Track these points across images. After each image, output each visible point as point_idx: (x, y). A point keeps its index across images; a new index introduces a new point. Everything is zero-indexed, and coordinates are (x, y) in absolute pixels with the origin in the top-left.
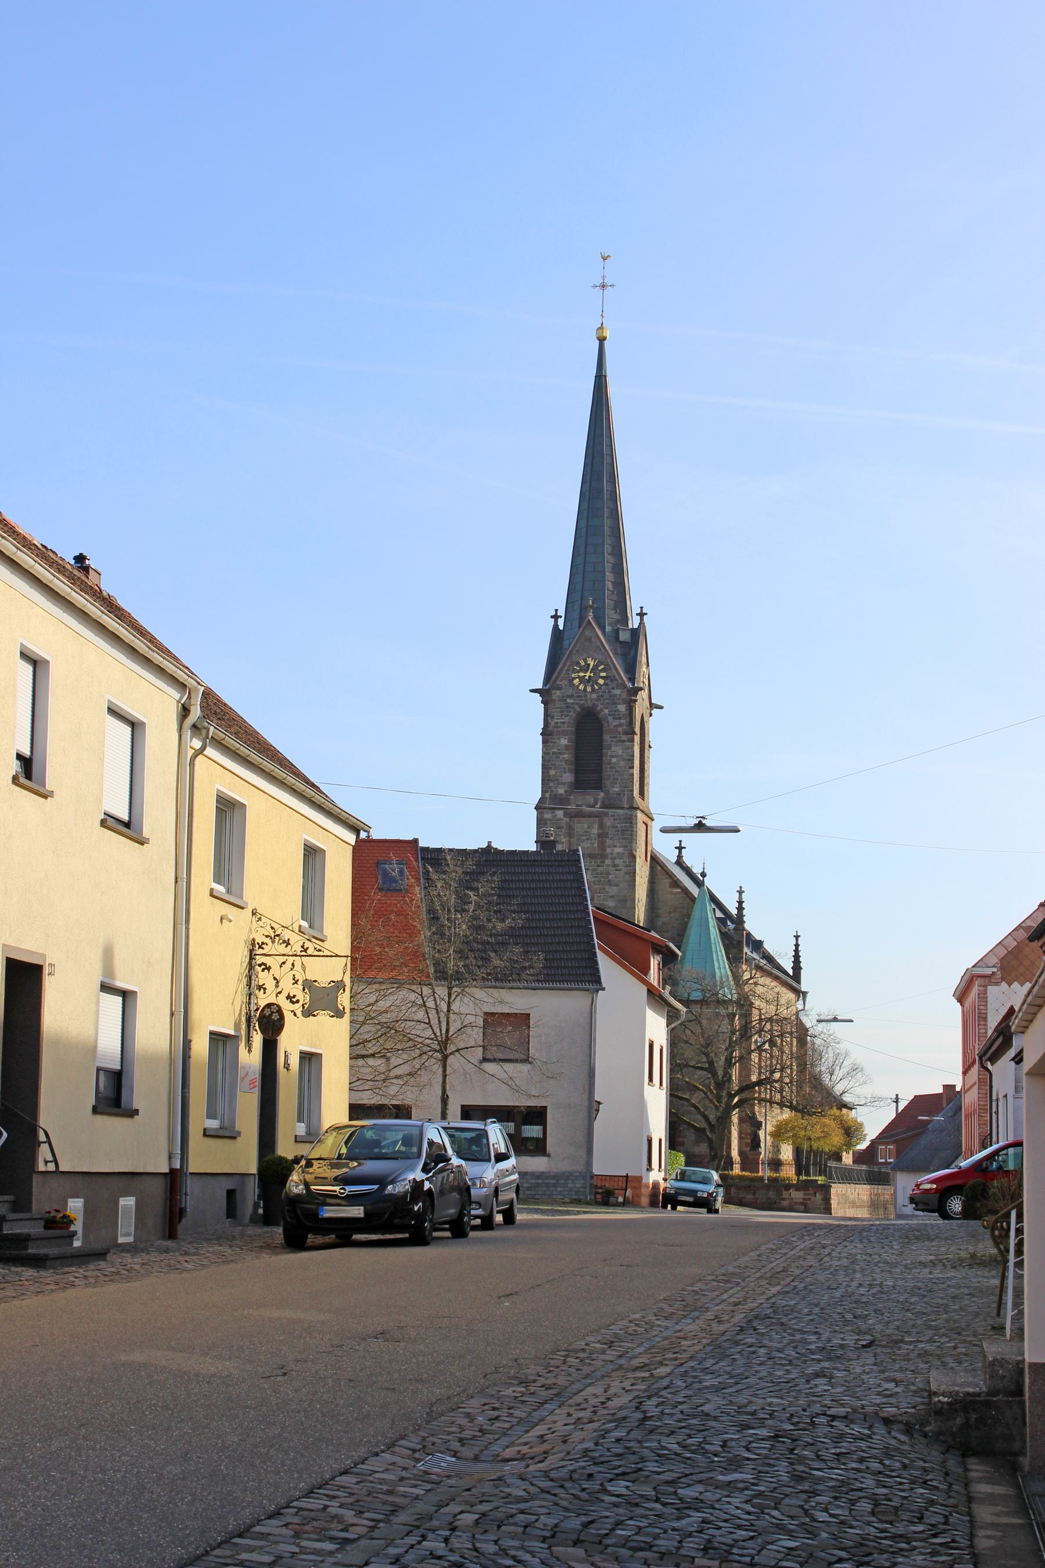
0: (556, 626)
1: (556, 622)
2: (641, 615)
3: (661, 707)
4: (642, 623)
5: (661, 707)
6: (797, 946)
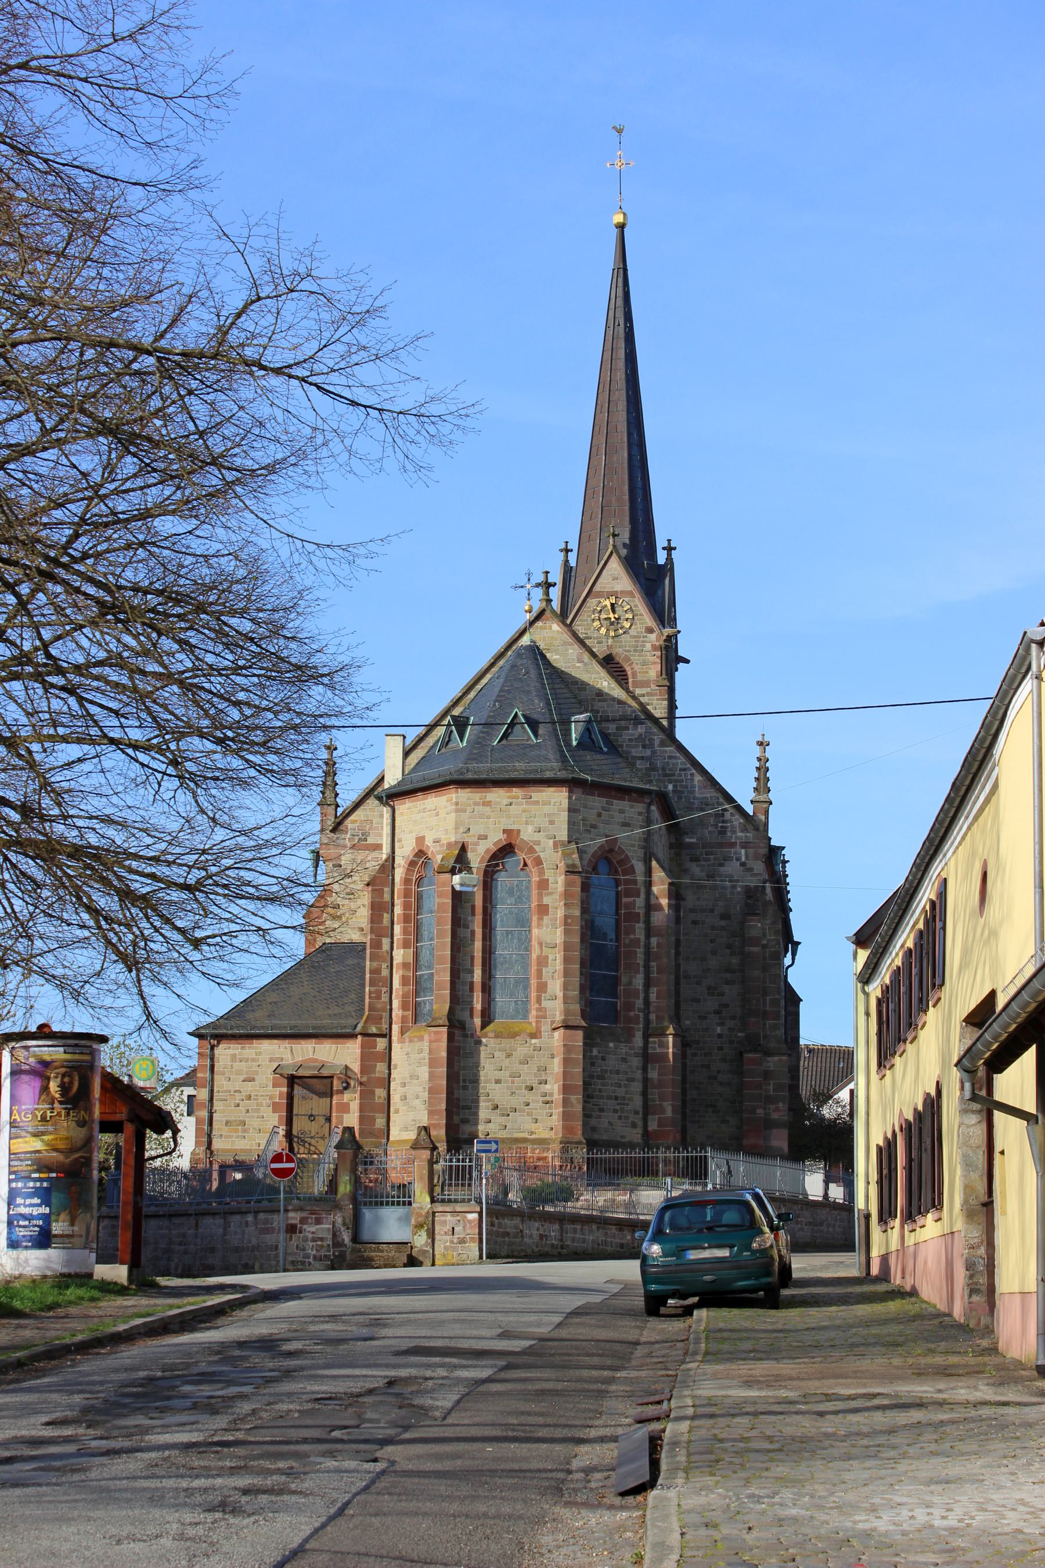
2: (669, 549)
3: (687, 661)
5: (687, 661)
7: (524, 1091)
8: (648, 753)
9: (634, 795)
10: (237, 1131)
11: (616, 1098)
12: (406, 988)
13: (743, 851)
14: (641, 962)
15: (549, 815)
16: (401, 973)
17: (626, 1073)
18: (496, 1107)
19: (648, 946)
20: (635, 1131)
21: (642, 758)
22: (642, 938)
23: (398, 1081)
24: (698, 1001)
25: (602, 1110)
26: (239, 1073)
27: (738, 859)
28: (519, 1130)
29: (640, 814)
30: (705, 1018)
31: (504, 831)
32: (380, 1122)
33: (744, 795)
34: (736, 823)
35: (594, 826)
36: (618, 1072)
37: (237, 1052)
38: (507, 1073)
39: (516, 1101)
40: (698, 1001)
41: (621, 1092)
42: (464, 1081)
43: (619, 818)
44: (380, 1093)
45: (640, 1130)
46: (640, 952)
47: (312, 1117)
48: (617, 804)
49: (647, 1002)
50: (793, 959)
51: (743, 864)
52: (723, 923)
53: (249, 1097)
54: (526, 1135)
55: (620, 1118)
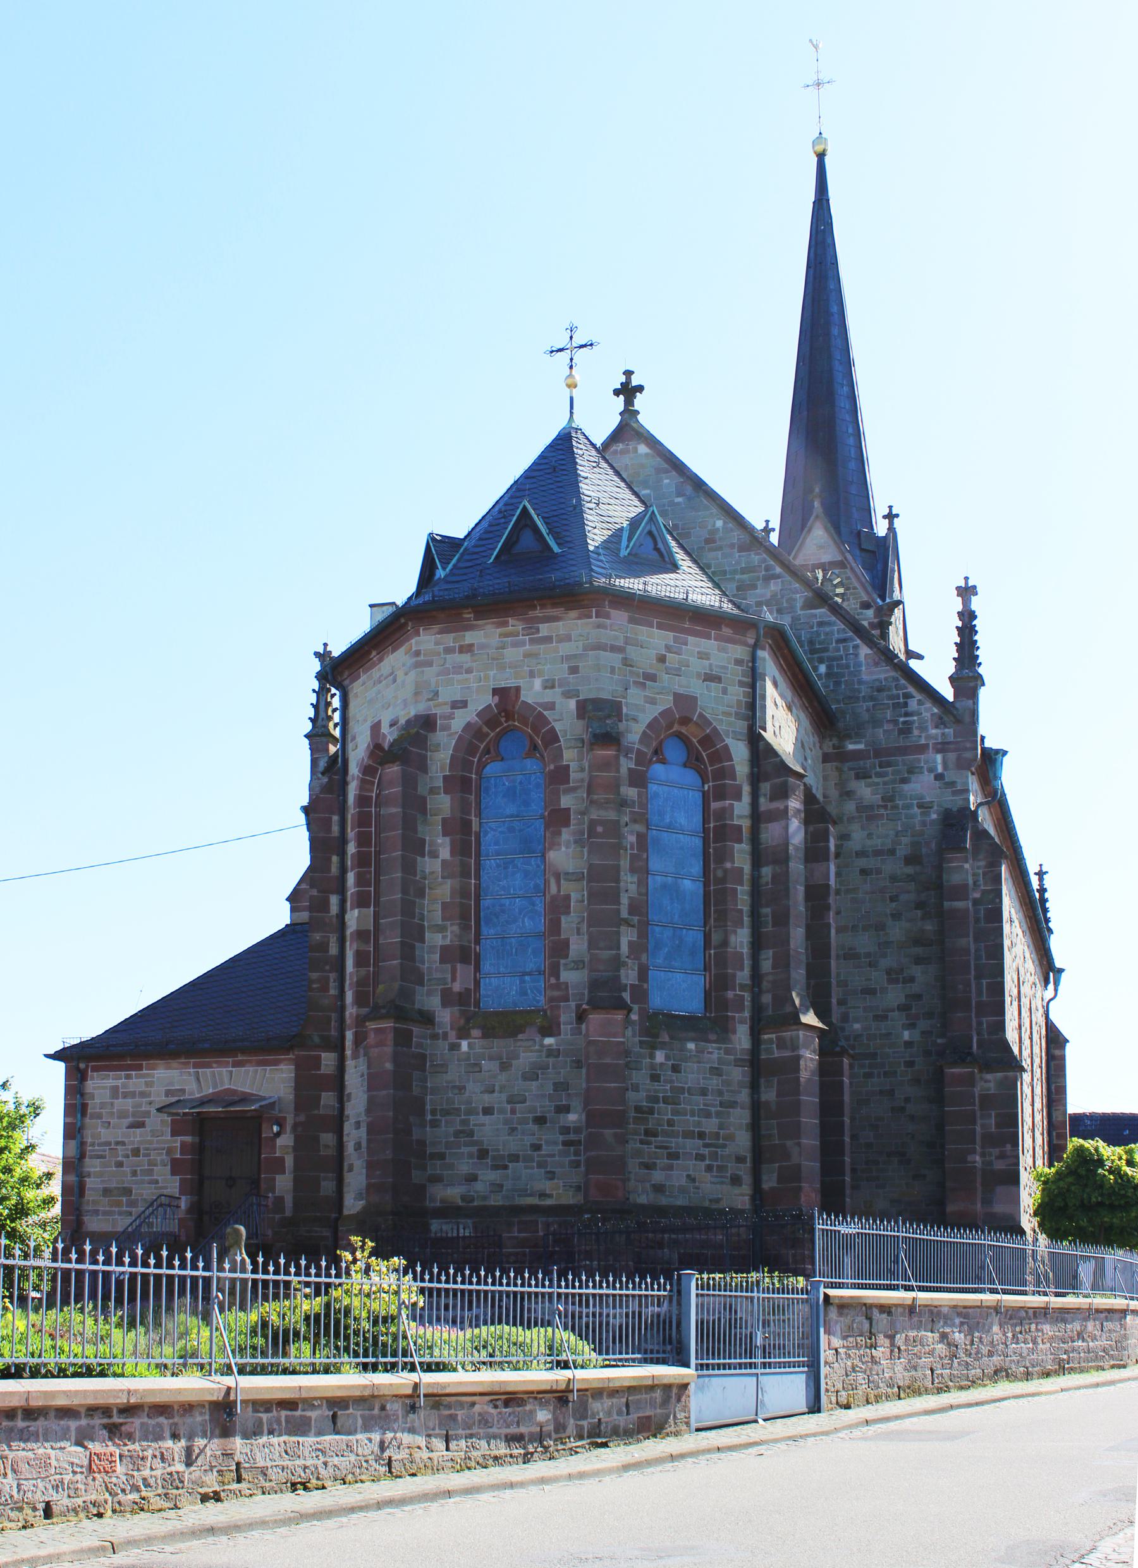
2: (891, 516)
4: (891, 529)
7: (532, 1126)
9: (727, 631)
10: (119, 1204)
12: (363, 971)
13: (939, 757)
14: (746, 909)
15: (568, 658)
16: (355, 946)
17: (720, 1093)
18: (483, 1154)
19: (755, 881)
20: (737, 1190)
23: (352, 1121)
24: (871, 992)
25: (674, 1156)
26: (122, 1115)
27: (930, 770)
28: (524, 1193)
29: (738, 662)
30: (885, 1018)
31: (495, 691)
32: (327, 1187)
33: (937, 670)
34: (927, 715)
35: (652, 678)
36: (704, 1092)
37: (119, 1083)
38: (504, 1097)
40: (871, 992)
41: (710, 1125)
42: (434, 1112)
43: (698, 666)
44: (328, 1138)
45: (746, 1189)
46: (743, 892)
47: (231, 1181)
48: (695, 644)
49: (756, 975)
50: (1056, 990)
51: (939, 777)
52: (910, 870)
53: (136, 1152)
54: (534, 1201)
55: (709, 1168)
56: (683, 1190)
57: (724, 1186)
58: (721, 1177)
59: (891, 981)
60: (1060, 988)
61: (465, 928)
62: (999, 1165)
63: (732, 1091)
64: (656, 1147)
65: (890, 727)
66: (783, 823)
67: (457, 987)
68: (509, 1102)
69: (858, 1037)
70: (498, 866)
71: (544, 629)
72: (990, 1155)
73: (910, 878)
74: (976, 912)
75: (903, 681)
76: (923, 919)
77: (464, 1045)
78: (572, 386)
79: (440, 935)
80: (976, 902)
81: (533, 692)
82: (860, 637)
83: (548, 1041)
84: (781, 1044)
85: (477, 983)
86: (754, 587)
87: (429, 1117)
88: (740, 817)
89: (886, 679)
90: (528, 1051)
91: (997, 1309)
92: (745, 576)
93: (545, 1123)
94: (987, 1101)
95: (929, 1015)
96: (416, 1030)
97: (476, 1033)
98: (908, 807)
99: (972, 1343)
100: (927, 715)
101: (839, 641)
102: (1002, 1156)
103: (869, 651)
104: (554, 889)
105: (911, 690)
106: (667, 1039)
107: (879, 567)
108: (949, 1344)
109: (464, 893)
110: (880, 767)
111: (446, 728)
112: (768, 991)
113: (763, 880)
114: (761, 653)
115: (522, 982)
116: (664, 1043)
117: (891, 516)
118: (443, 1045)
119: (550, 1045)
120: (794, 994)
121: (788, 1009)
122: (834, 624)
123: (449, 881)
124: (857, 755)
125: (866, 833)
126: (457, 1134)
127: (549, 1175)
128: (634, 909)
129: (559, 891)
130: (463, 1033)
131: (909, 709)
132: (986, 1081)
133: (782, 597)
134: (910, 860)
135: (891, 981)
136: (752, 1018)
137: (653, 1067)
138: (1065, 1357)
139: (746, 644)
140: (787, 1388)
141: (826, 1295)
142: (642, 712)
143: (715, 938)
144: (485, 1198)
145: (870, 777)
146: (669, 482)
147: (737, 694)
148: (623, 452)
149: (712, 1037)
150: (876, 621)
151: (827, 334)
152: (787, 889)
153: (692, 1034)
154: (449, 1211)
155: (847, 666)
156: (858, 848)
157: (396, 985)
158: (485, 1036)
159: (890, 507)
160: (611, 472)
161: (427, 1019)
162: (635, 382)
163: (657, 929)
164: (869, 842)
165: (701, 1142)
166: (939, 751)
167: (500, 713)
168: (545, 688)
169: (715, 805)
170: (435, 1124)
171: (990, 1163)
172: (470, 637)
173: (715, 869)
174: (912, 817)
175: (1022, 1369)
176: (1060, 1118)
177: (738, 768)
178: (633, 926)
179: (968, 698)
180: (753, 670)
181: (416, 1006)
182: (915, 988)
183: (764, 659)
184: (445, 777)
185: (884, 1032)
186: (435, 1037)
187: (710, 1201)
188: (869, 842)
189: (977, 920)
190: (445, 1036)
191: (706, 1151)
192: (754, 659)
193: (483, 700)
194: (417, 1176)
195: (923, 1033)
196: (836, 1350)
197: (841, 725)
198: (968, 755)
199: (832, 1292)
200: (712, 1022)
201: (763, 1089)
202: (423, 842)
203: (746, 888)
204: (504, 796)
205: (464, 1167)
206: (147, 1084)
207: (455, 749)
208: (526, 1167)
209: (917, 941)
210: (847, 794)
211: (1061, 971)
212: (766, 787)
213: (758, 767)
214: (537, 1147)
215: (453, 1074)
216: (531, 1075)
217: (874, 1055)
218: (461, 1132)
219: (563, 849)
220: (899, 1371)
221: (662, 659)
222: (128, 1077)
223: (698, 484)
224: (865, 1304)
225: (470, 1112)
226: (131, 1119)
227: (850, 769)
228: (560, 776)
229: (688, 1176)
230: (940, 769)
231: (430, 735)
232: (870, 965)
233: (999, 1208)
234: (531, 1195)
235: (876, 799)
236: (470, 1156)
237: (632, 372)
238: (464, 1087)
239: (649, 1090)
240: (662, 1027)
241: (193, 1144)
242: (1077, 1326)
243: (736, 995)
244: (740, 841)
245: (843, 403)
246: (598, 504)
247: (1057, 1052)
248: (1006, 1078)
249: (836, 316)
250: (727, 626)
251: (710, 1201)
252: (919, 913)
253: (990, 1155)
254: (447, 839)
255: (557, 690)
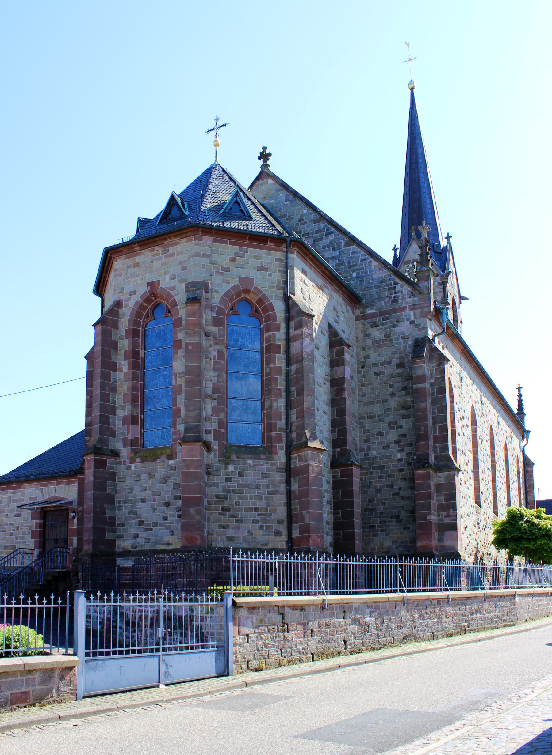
0: (395, 255)
1: (395, 252)
2: (448, 237)
3: (467, 299)
4: (449, 243)
5: (467, 299)
6: (520, 396)
7: (164, 508)
8: (337, 253)
9: (270, 244)
11: (256, 510)
14: (283, 388)
17: (268, 487)
18: (141, 523)
20: (278, 538)
21: (333, 258)
22: (283, 367)
24: (381, 434)
27: (408, 320)
29: (277, 260)
34: (405, 292)
35: (228, 270)
36: (258, 486)
37: (11, 495)
38: (150, 493)
39: (156, 517)
40: (381, 434)
41: (261, 504)
42: (119, 503)
45: (284, 537)
47: (56, 541)
49: (288, 422)
50: (527, 441)
51: (412, 322)
52: (399, 371)
53: (18, 528)
55: (261, 527)
56: (245, 539)
57: (270, 537)
58: (268, 532)
59: (391, 428)
60: (529, 439)
61: (134, 406)
62: (447, 521)
63: (275, 486)
64: (229, 517)
65: (388, 300)
66: (300, 341)
67: (130, 437)
68: (153, 495)
69: (374, 458)
70: (152, 373)
71: (171, 250)
72: (442, 515)
73: (399, 375)
74: (432, 389)
75: (393, 276)
76: (406, 395)
77: (133, 466)
78: (217, 145)
79: (123, 411)
80: (432, 385)
81: (165, 283)
82: (372, 257)
83: (171, 462)
84: (300, 459)
85: (142, 435)
86: (322, 239)
87: (117, 505)
88: (278, 340)
89: (385, 276)
90: (162, 467)
91: (403, 601)
92: (318, 234)
93: (169, 505)
94: (439, 487)
95: (410, 444)
96: (109, 460)
97: (138, 460)
98: (397, 339)
99: (382, 622)
100: (405, 292)
101: (362, 260)
102: (448, 516)
103: (377, 263)
104: (174, 383)
105: (397, 280)
106: (235, 458)
107: (443, 259)
108: (361, 625)
109: (134, 388)
110: (383, 320)
111: (127, 305)
112: (294, 431)
113: (292, 373)
114: (290, 255)
115: (163, 432)
116: (234, 460)
117: (448, 237)
118: (123, 467)
119: (172, 464)
120: (306, 431)
121: (304, 440)
122: (359, 252)
123: (127, 383)
124: (372, 316)
125: (377, 354)
126: (130, 513)
127: (171, 533)
128: (215, 390)
129: (176, 383)
130: (132, 461)
131: (397, 290)
132: (439, 477)
133: (335, 242)
134: (398, 366)
135: (391, 428)
136: (286, 446)
137: (227, 474)
138: (466, 624)
139: (282, 251)
140: (205, 660)
141: (233, 600)
142: (220, 288)
143: (267, 405)
144: (142, 546)
145: (378, 326)
146: (283, 194)
147: (278, 277)
148: (261, 185)
149: (263, 457)
150: (441, 282)
151: (417, 162)
152: (303, 376)
153: (250, 456)
154: (126, 554)
155: (366, 272)
156: (373, 362)
157: (97, 437)
158: (142, 461)
159: (448, 233)
160: (229, 180)
161: (115, 454)
162: (267, 151)
163: (233, 401)
164: (379, 359)
165: (256, 513)
166: (411, 310)
167: (151, 295)
168: (171, 279)
169: (266, 335)
170: (120, 508)
171: (442, 520)
172: (139, 259)
173: (266, 368)
174: (400, 344)
175: (429, 634)
176: (532, 499)
177: (278, 315)
178: (215, 399)
179: (426, 281)
180: (286, 263)
181: (110, 448)
182: (402, 431)
183: (293, 258)
184: (126, 330)
185: (387, 454)
186: (120, 463)
187: (262, 544)
188: (379, 359)
189: (433, 394)
190: (125, 461)
191: (259, 518)
192: (286, 258)
193: (143, 289)
194: (109, 536)
195: (407, 454)
196: (247, 635)
197: (364, 301)
198: (426, 310)
199: (239, 600)
200: (264, 450)
201: (292, 484)
202: (115, 364)
203: (283, 377)
204: (155, 338)
205: (133, 530)
206: (22, 496)
207: (131, 316)
208: (161, 530)
209: (403, 407)
210: (367, 335)
211: (529, 432)
212: (292, 324)
213: (289, 313)
214: (165, 519)
215: (128, 482)
216: (164, 481)
217: (383, 467)
218: (132, 512)
219: (178, 361)
220: (313, 644)
221: (233, 260)
222: (15, 492)
223: (295, 194)
224: (277, 606)
225: (135, 502)
226: (16, 513)
227: (369, 323)
228: (177, 323)
229: (248, 532)
230: (412, 319)
231: (120, 310)
232: (380, 421)
233: (447, 543)
234: (162, 544)
235: (382, 337)
236: (135, 525)
237: (266, 148)
238: (133, 489)
239: (225, 486)
240: (232, 452)
241: (40, 523)
242: (475, 606)
243: (276, 434)
244: (279, 352)
245: (424, 190)
246: (215, 193)
247: (529, 469)
248: (449, 474)
249: (421, 155)
250: (270, 241)
251: (262, 544)
252: (404, 392)
253: (442, 515)
254: (126, 361)
255: (177, 279)
